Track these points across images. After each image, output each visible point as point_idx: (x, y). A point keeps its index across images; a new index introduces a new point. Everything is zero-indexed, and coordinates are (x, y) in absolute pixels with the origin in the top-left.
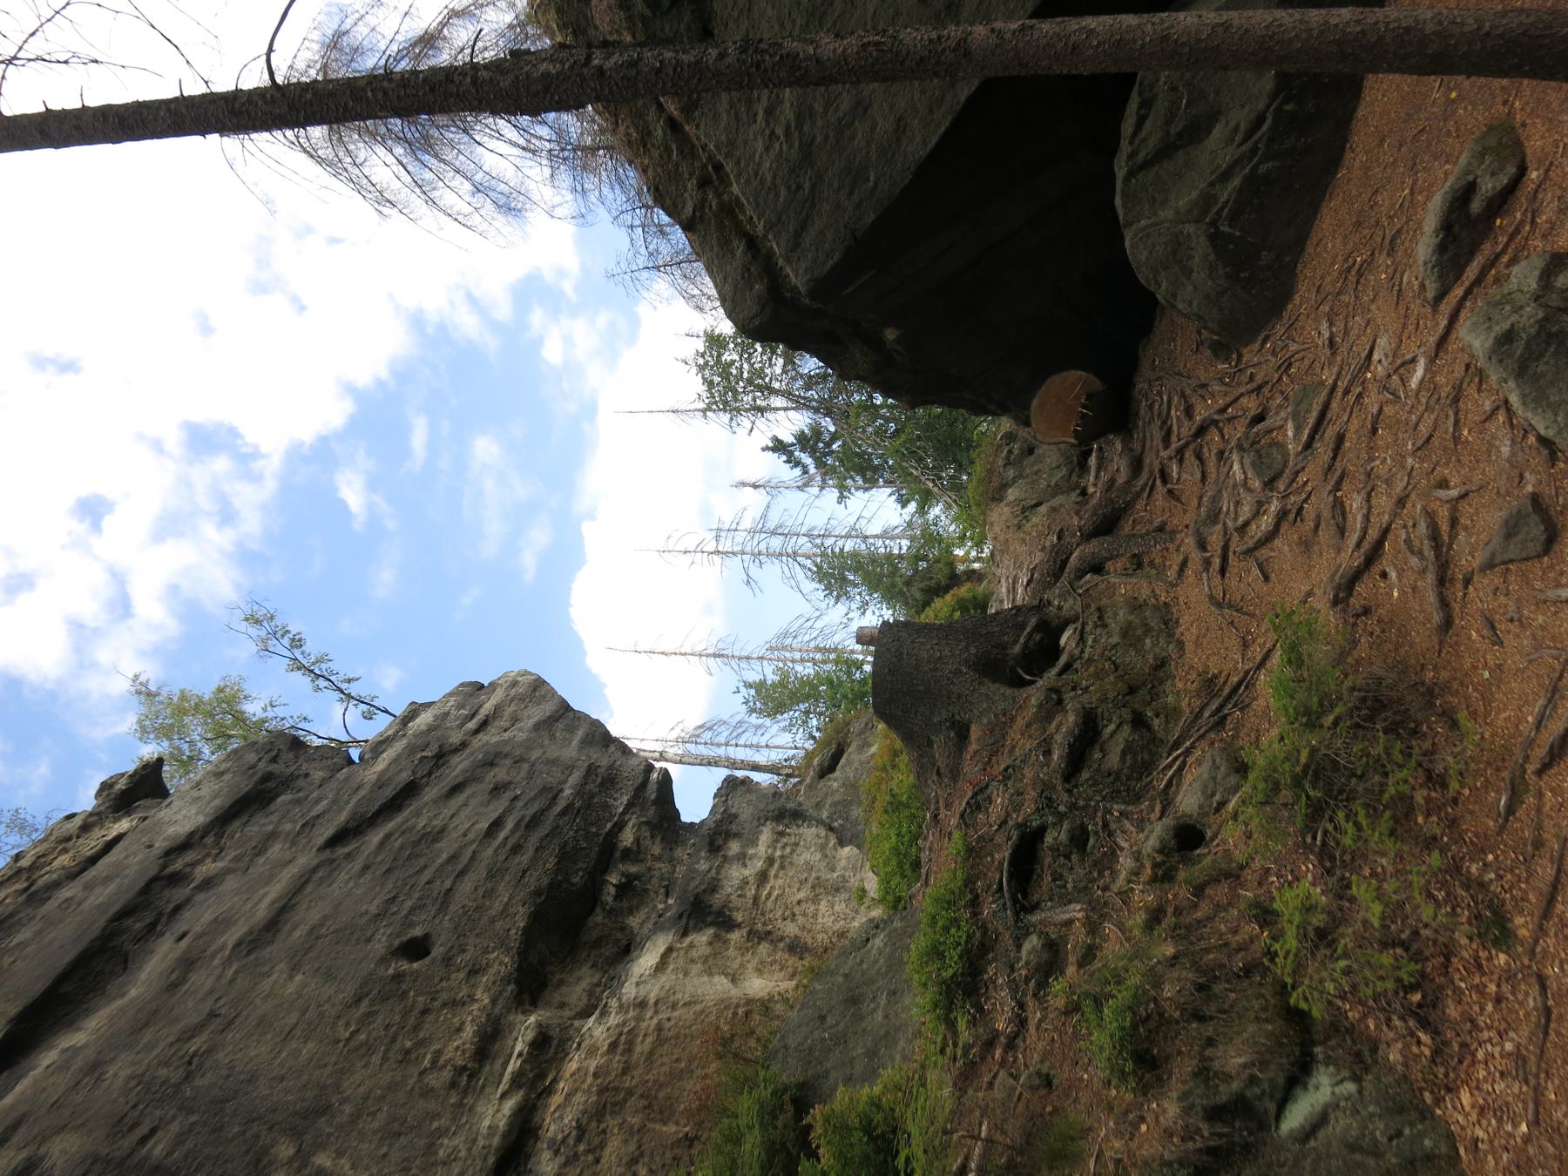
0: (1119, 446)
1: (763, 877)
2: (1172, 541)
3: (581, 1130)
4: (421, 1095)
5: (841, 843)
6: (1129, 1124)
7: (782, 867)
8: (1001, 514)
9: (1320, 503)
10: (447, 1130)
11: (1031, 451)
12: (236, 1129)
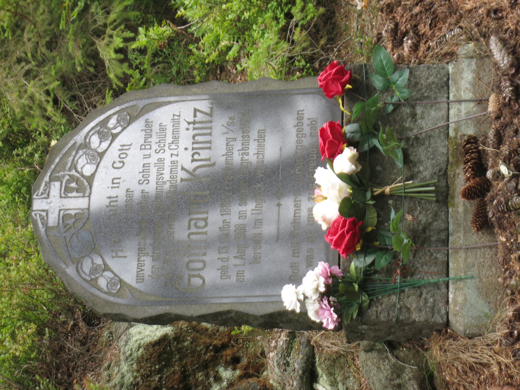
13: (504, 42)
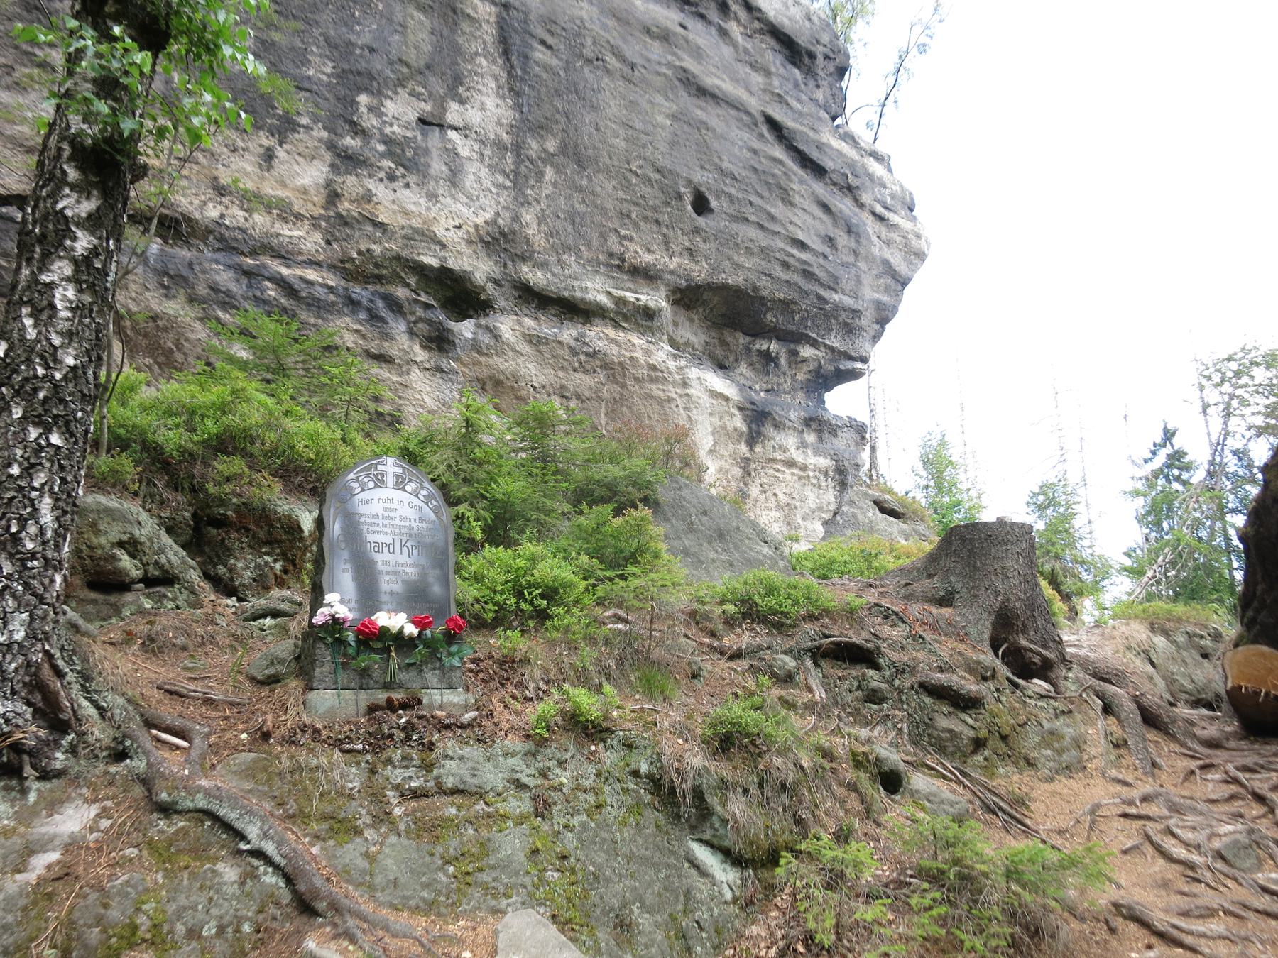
0: (1228, 729)
1: (791, 464)
2: (1145, 774)
3: (593, 355)
6: (684, 732)
8: (1139, 632)
9: (1208, 898)
10: (581, 258)
11: (1205, 656)
12: (560, 106)
13: (475, 719)
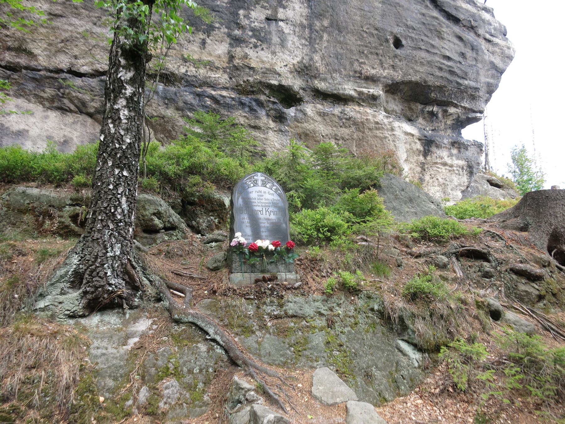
1: (445, 164)
3: (349, 119)
4: (350, 62)
5: (463, 192)
6: (394, 291)
7: (450, 171)
12: (329, 4)
